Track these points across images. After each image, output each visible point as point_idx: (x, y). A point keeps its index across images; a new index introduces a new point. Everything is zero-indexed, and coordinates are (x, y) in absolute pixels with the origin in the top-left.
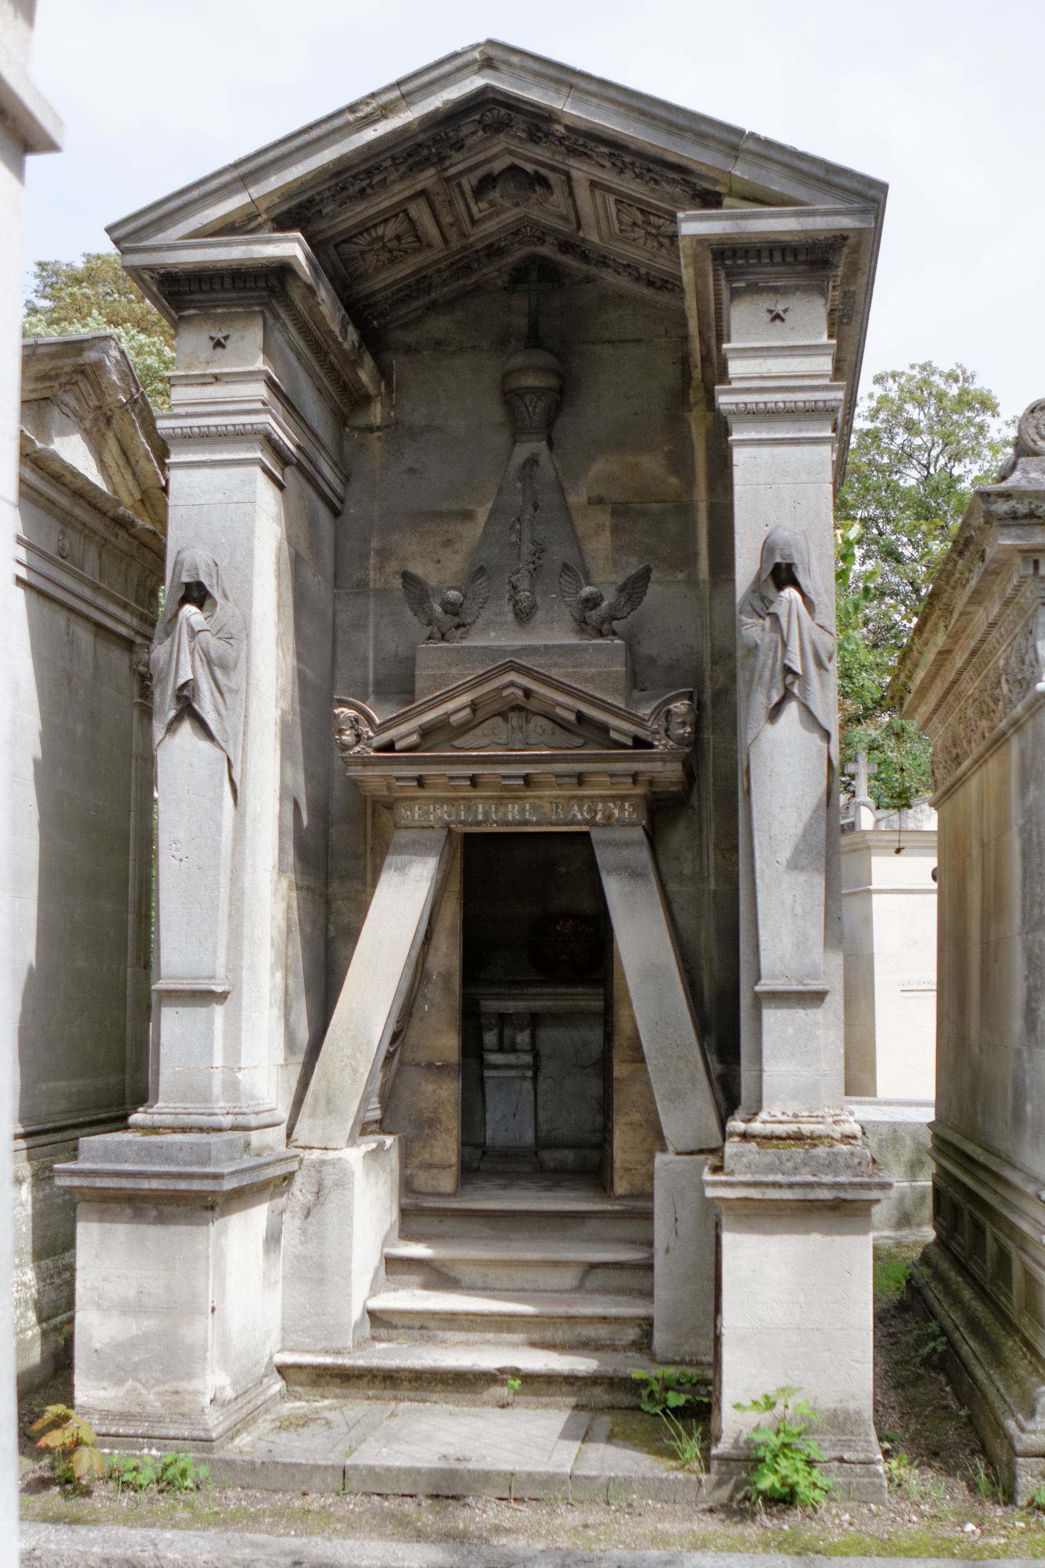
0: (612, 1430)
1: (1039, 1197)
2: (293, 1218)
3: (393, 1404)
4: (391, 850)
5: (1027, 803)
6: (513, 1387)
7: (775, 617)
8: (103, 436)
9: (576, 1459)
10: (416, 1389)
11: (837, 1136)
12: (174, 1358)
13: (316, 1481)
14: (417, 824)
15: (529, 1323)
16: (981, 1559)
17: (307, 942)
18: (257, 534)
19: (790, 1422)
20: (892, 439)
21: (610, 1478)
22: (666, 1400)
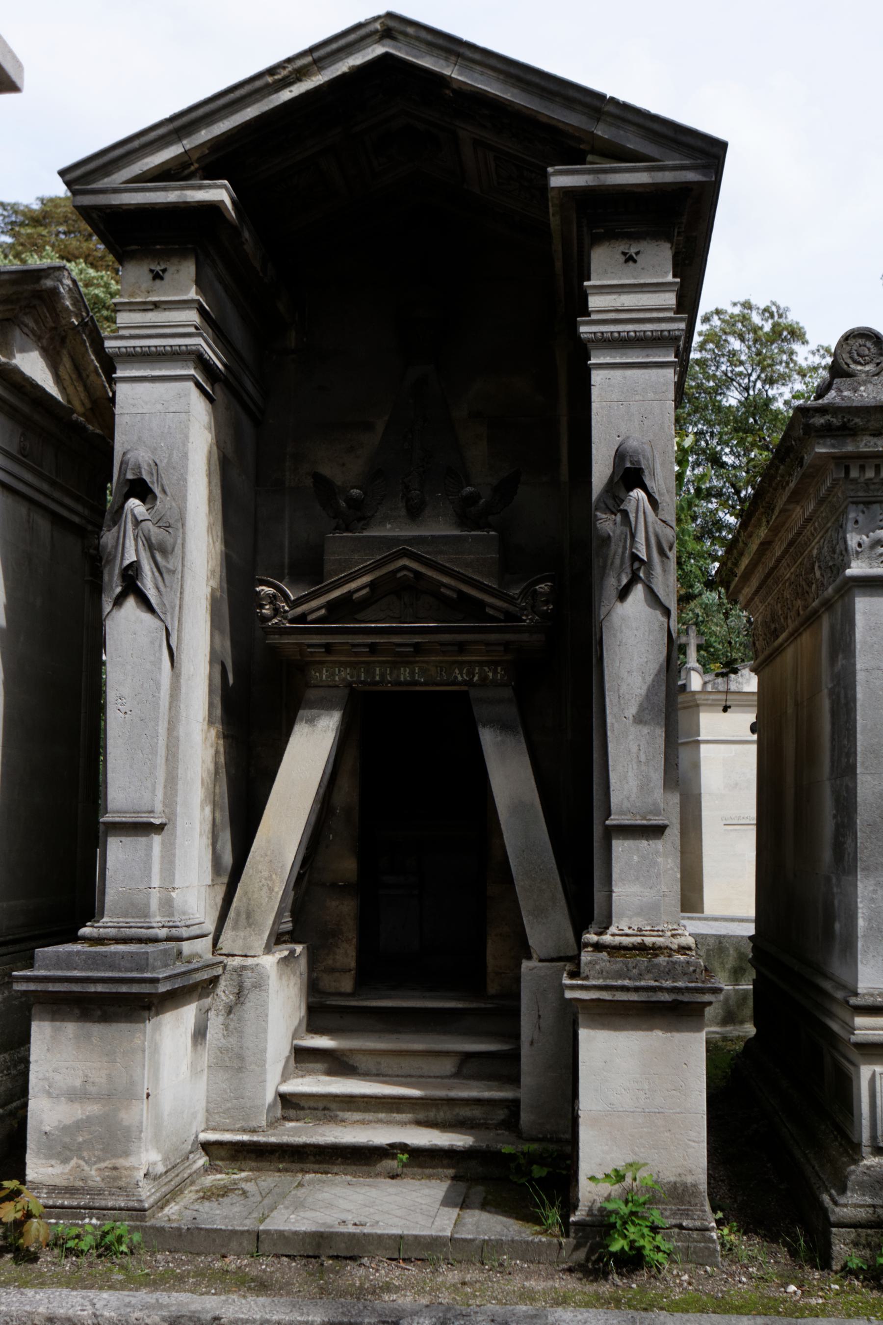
0: (485, 1198)
1: (847, 1002)
2: (217, 1015)
3: (300, 1176)
5: (836, 670)
6: (401, 1160)
7: (625, 514)
9: (455, 1224)
10: (320, 1163)
11: (675, 947)
12: (113, 1139)
13: (234, 1245)
15: (416, 1104)
16: (803, 1317)
18: (191, 440)
19: (636, 1194)
20: (717, 367)
21: (484, 1240)
22: (531, 1172)
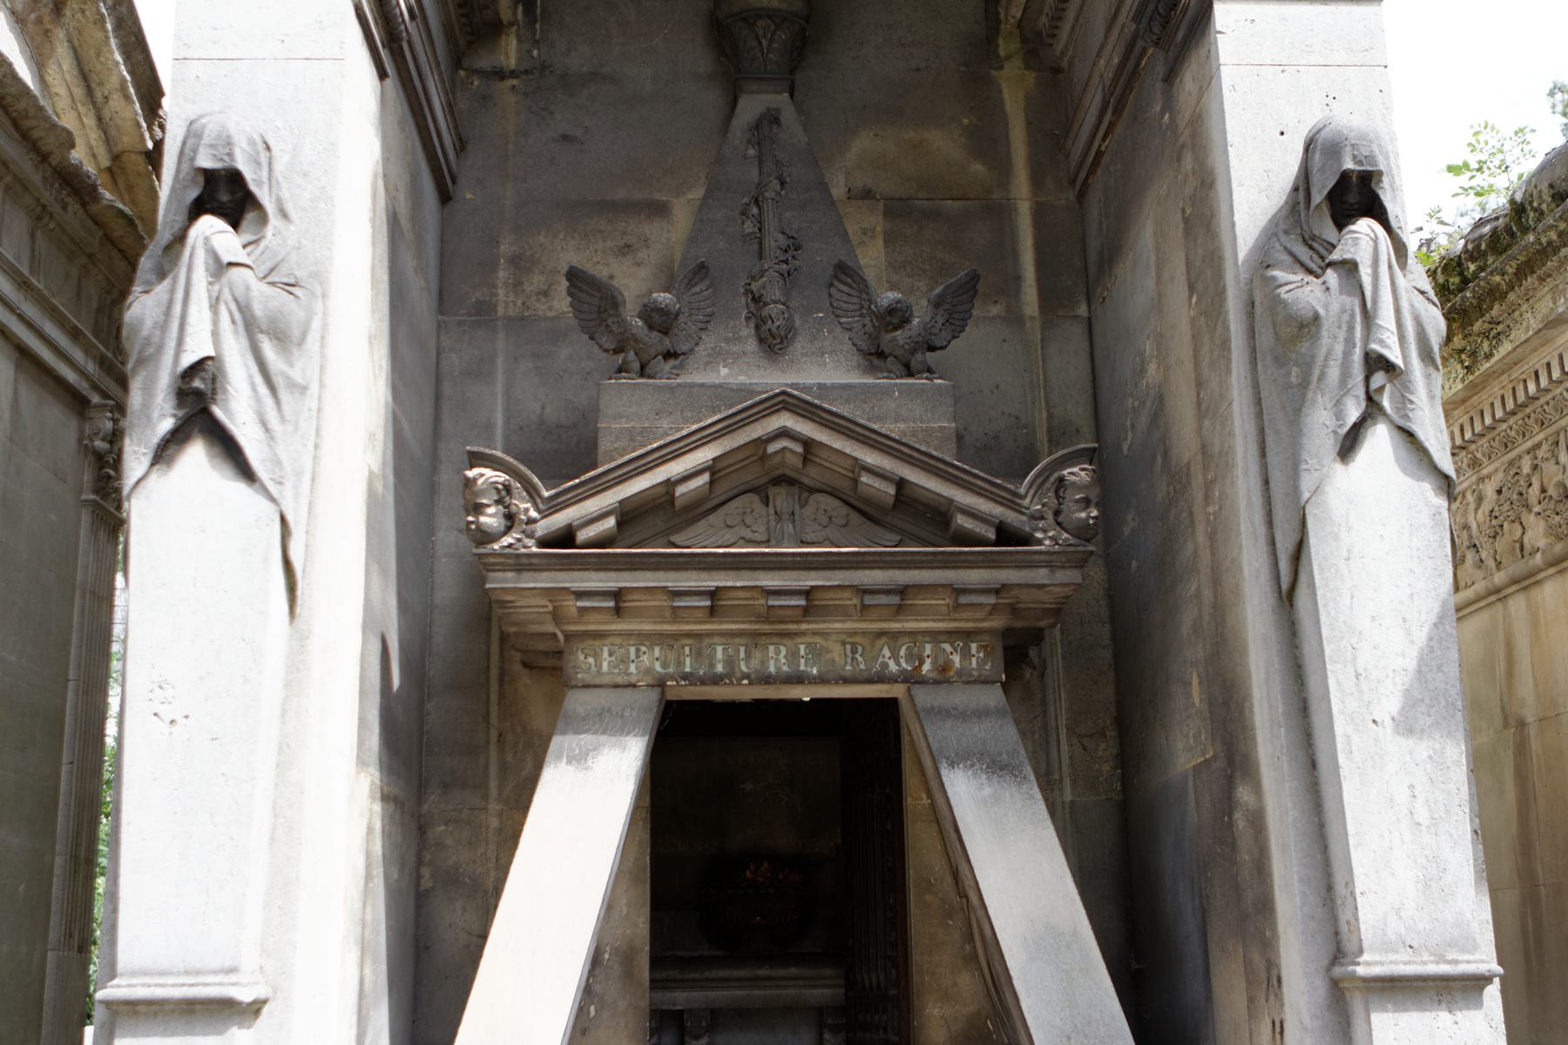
4: (560, 725)
8: (47, 33)
14: (606, 680)
17: (394, 897)
